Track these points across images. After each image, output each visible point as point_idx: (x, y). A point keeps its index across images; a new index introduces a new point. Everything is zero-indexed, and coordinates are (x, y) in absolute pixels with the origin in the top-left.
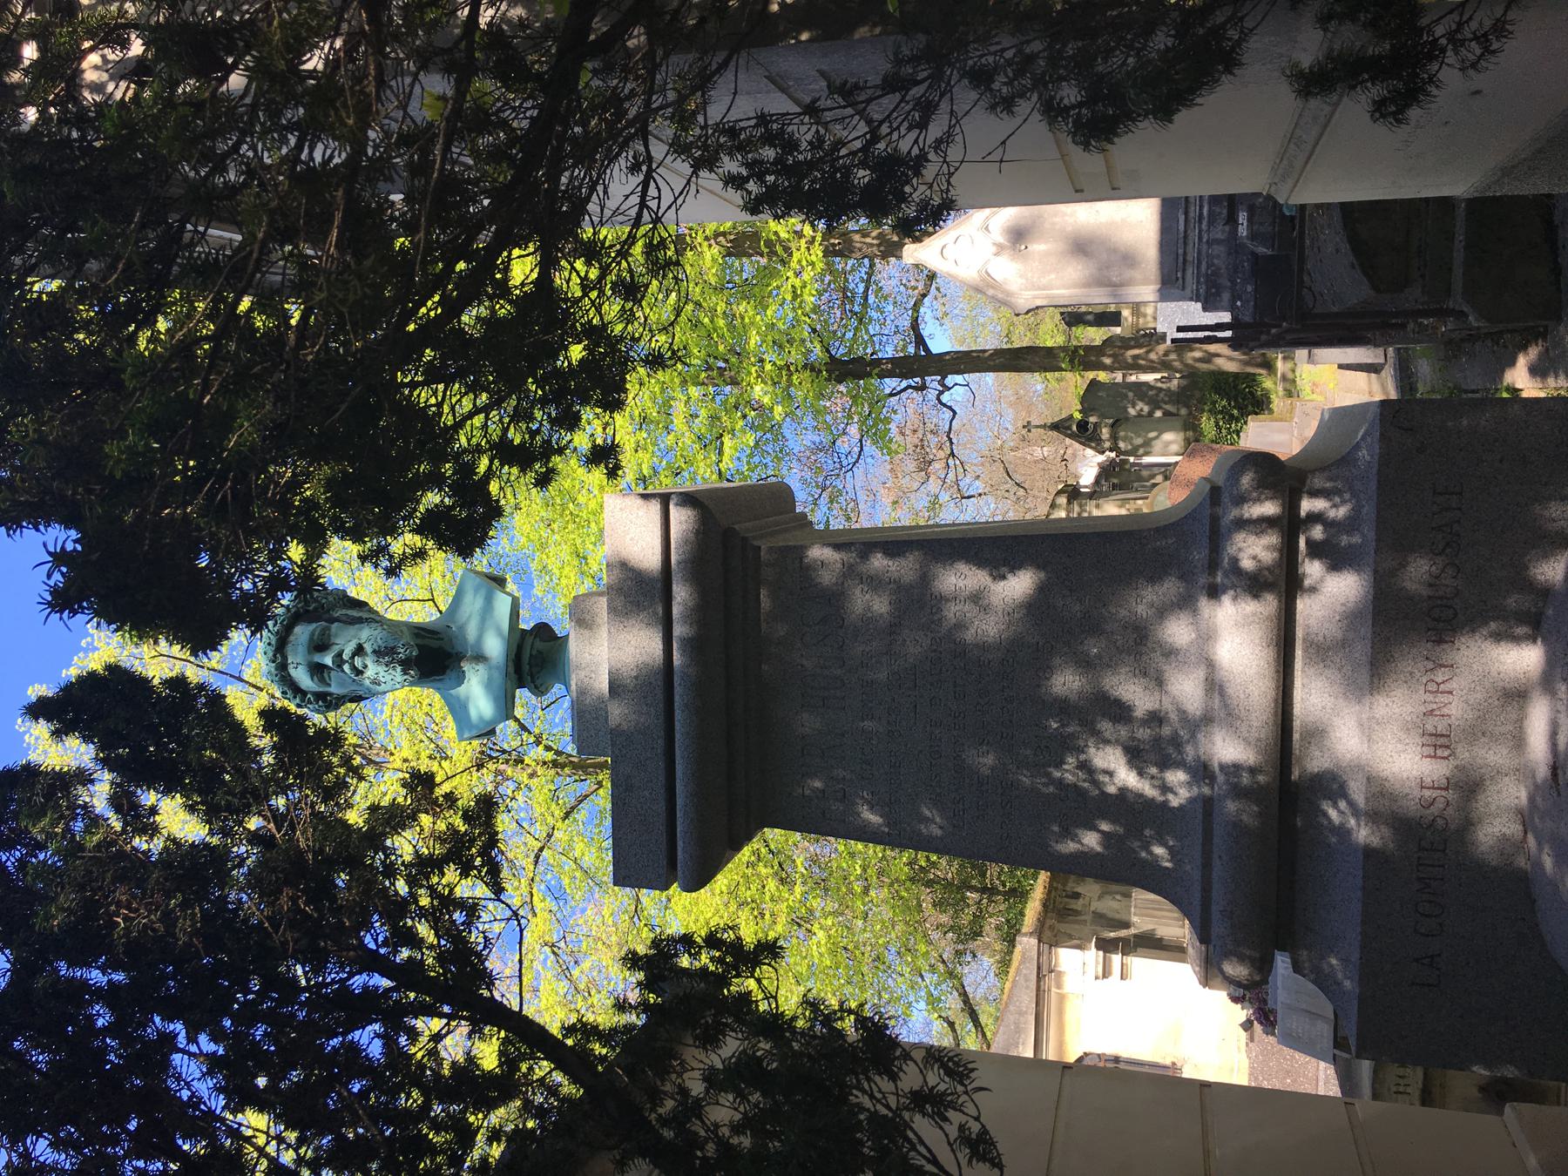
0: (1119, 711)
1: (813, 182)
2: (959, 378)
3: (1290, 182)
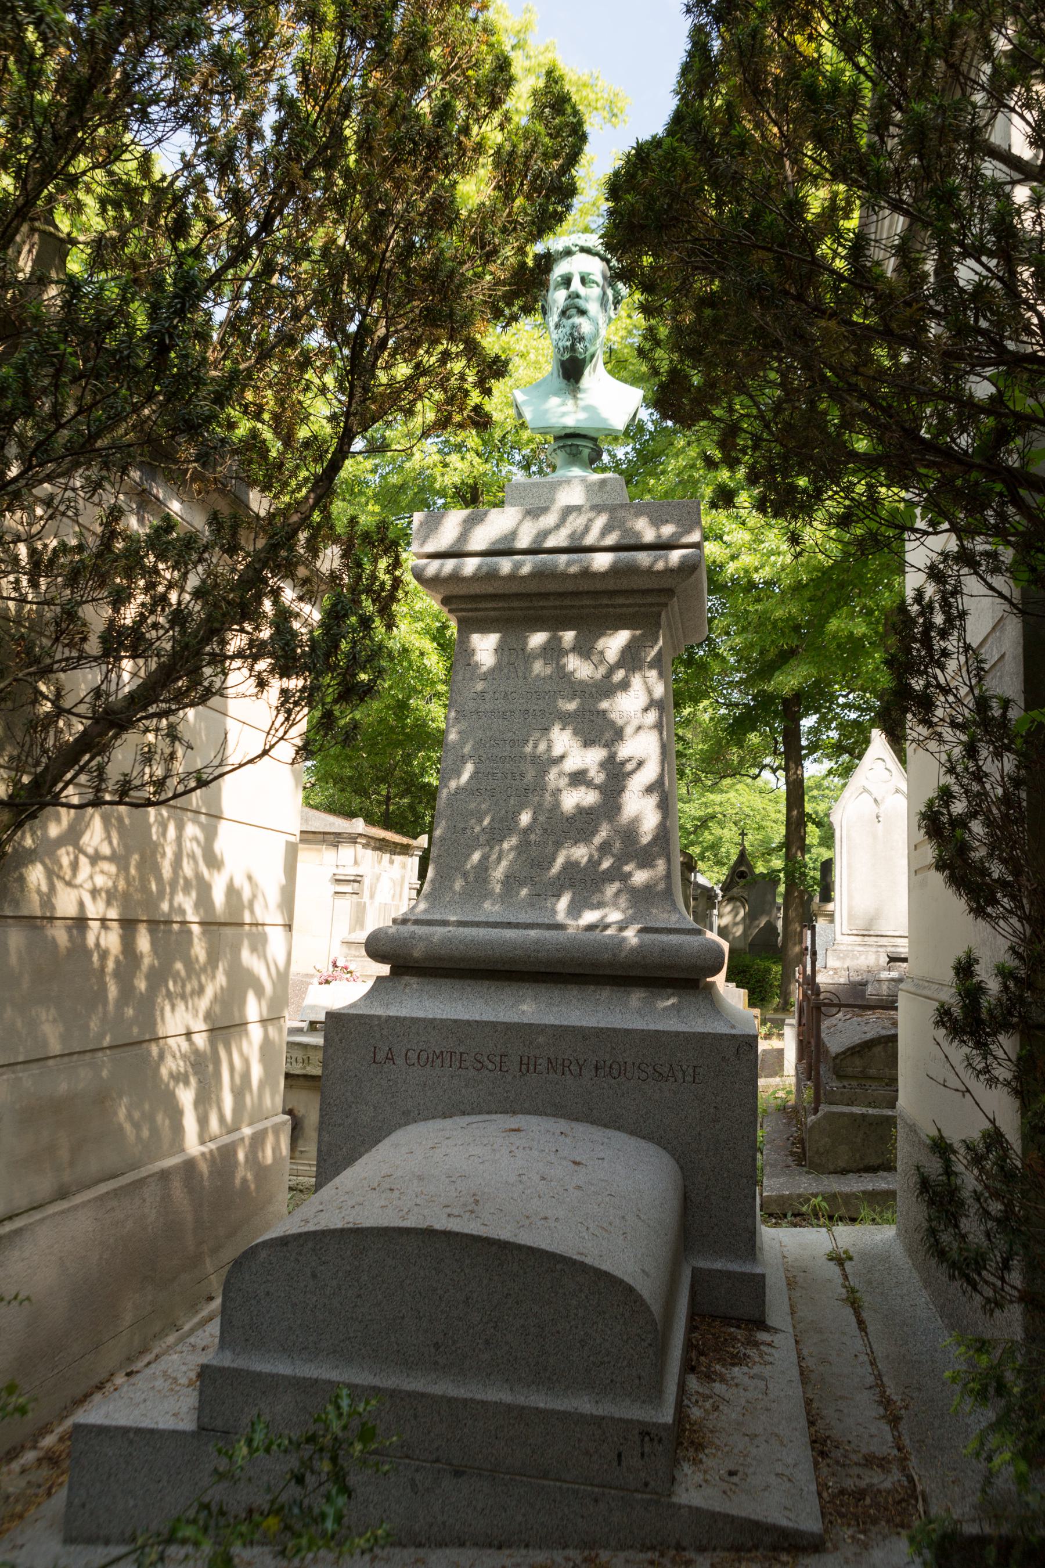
1: (918, 650)
2: (783, 780)
3: (912, 989)
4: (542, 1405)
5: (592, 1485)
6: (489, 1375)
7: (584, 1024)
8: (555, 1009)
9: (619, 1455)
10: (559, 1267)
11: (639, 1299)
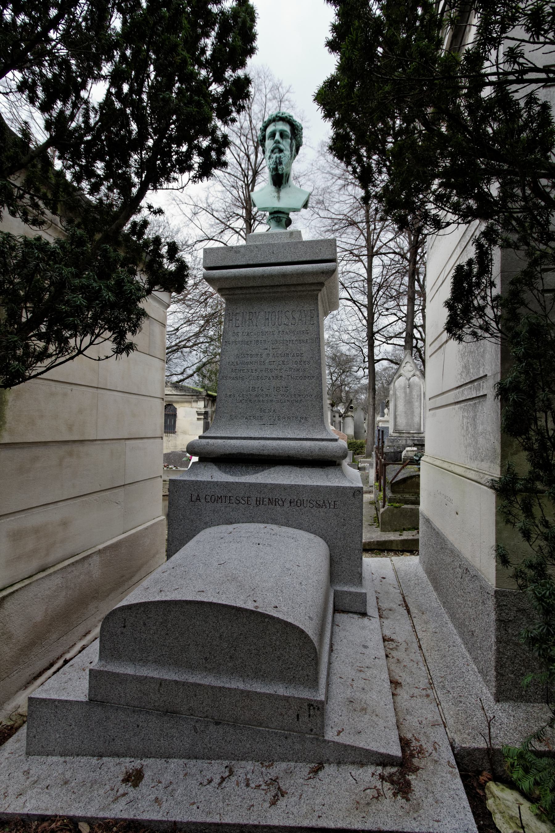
0: (57, 126)
4: (258, 690)
5: (284, 730)
6: (232, 674)
7: (285, 483)
8: (272, 476)
9: (298, 715)
10: (267, 620)
11: (307, 636)
